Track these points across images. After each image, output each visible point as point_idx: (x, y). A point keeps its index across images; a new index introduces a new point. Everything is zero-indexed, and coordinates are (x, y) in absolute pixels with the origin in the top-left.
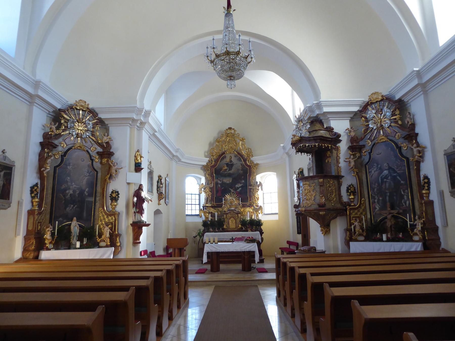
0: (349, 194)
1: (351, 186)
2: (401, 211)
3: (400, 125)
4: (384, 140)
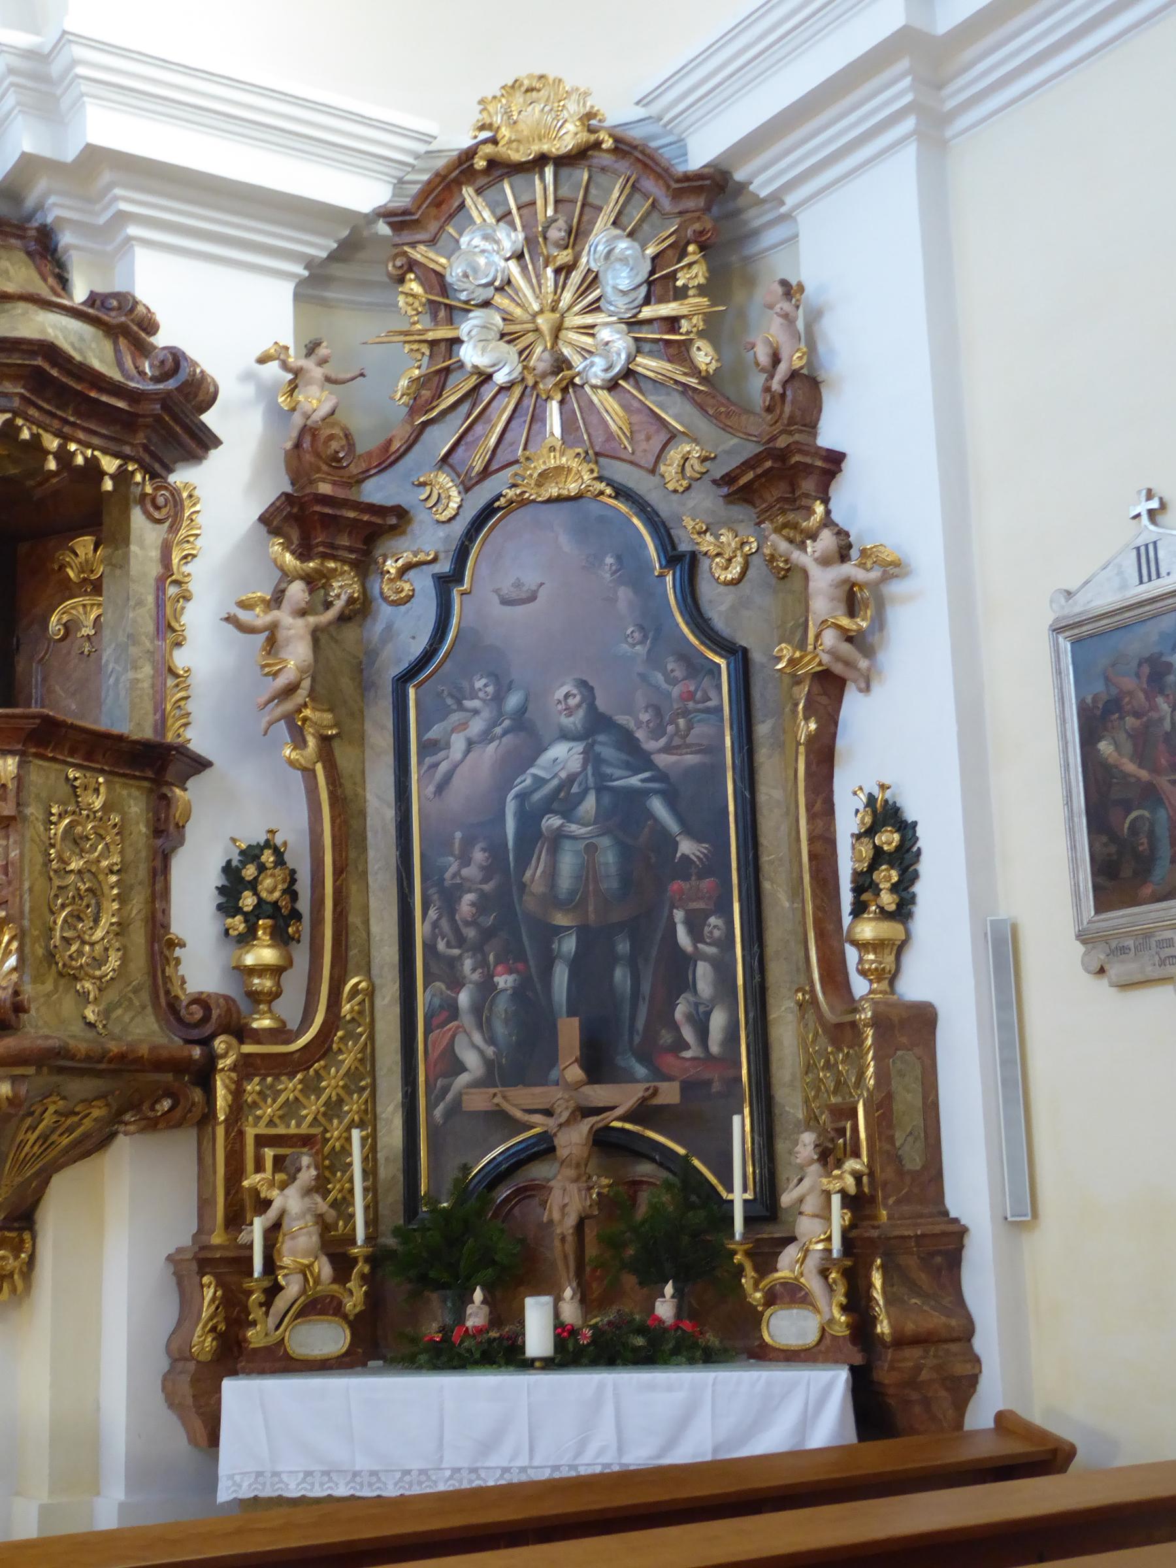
0: (238, 924)
1: (268, 857)
2: (669, 1094)
3: (705, 379)
4: (572, 488)
